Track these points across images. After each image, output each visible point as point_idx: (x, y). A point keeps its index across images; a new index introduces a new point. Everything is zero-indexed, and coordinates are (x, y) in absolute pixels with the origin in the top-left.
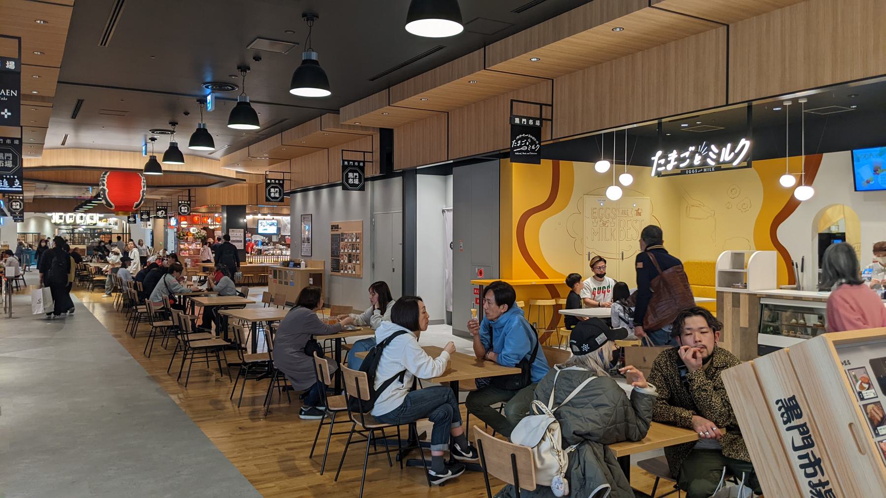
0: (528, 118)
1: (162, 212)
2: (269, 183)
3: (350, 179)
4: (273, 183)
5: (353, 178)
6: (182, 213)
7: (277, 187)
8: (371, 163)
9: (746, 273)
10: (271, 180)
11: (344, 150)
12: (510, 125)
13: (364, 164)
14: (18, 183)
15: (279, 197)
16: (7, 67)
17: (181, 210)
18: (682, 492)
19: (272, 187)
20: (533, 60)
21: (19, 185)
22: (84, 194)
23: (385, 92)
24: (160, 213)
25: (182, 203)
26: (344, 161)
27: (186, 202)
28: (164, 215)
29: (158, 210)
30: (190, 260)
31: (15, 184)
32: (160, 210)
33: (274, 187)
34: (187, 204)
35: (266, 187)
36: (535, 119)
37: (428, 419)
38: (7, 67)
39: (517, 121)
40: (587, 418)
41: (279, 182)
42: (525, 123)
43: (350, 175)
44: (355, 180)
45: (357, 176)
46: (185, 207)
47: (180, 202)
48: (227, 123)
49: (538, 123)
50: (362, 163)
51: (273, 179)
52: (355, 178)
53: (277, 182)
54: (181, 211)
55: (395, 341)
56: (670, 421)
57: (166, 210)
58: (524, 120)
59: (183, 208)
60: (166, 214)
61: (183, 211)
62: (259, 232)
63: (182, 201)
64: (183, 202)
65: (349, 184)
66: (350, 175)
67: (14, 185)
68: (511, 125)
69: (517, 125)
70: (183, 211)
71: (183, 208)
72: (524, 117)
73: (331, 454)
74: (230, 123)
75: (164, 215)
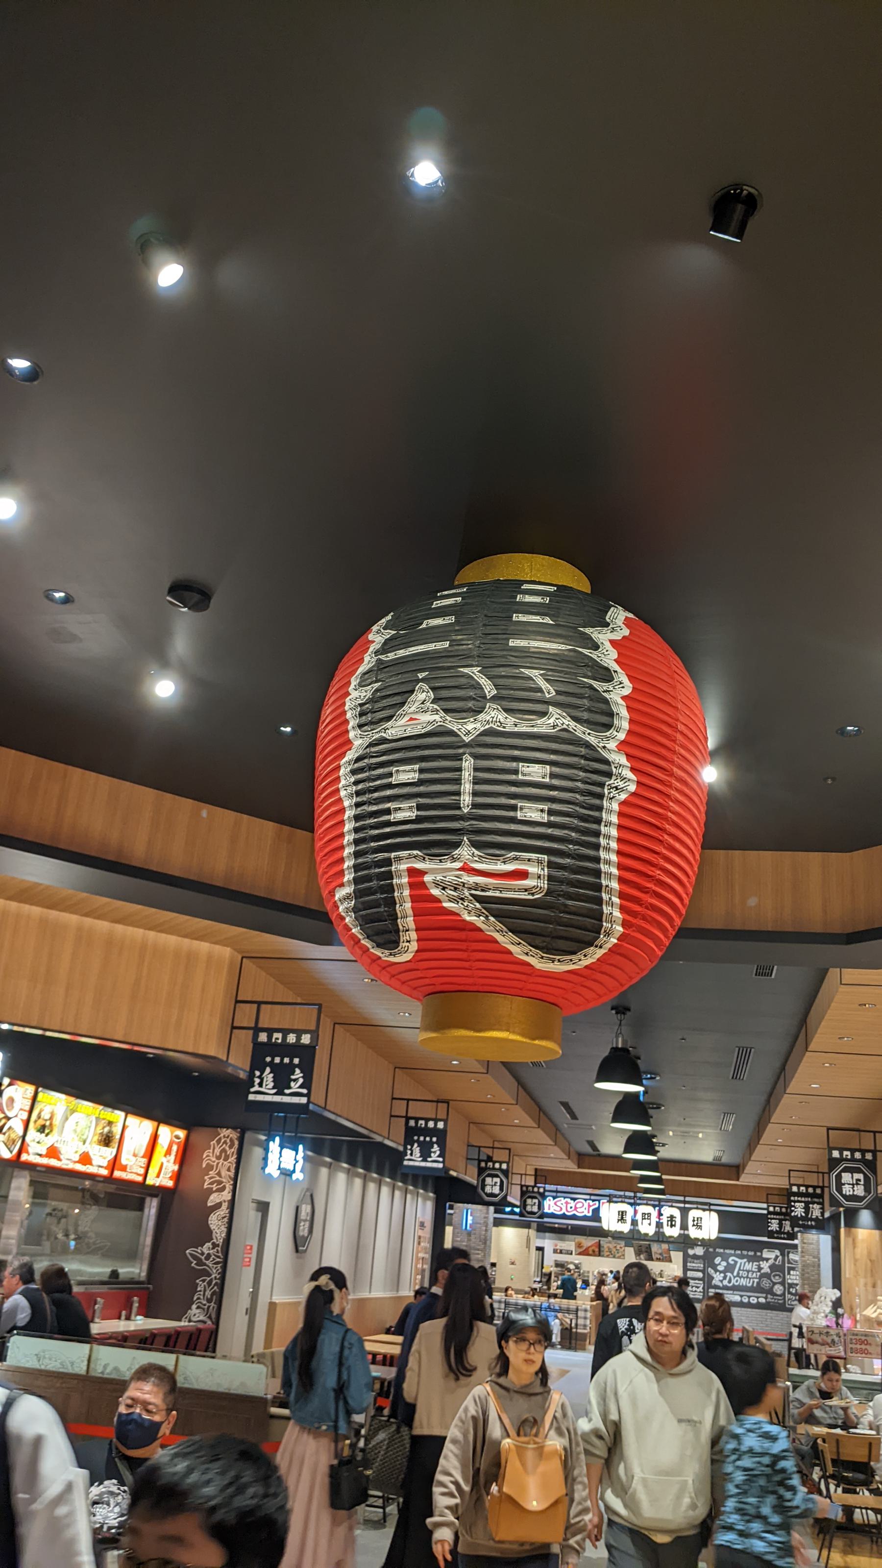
2: (836, 1159)
4: (847, 1160)
5: (853, 1185)
6: (845, 1197)
7: (859, 1171)
9: (590, 1230)
13: (875, 1156)
14: (438, 1153)
15: (864, 1197)
16: (302, 1041)
17: (840, 1185)
19: (845, 1170)
21: (439, 1156)
22: (817, 1473)
25: (841, 1160)
27: (858, 1155)
31: (292, 1084)
33: (852, 1170)
34: (863, 1161)
38: (302, 1041)
41: (863, 1155)
44: (855, 1188)
45: (860, 1180)
46: (857, 1176)
47: (836, 1154)
48: (594, 1075)
50: (870, 1154)
51: (847, 1150)
52: (857, 1184)
53: (858, 1155)
54: (839, 1190)
56: (316, 1147)
59: (846, 1177)
61: (847, 1190)
63: (841, 1150)
64: (846, 1154)
67: (290, 1088)
70: (847, 1190)
71: (846, 1177)
73: (872, 1361)
74: (600, 1079)
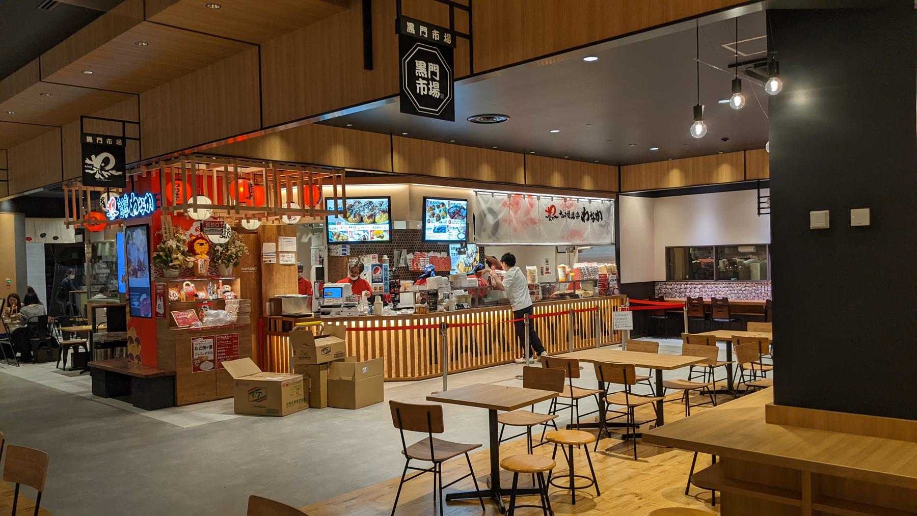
0: (431, 27)
1: (106, 161)
3: (421, 81)
8: (6, 171)
10: (94, 136)
11: (61, 129)
12: (81, 144)
18: (590, 475)
20: (47, 95)
23: (35, 63)
24: (96, 161)
26: (84, 135)
27: (436, 35)
28: (111, 170)
29: (90, 150)
30: (210, 341)
32: (96, 149)
35: (403, 51)
36: (442, 31)
37: (89, 373)
39: (411, 28)
40: (607, 450)
42: (426, 36)
43: (421, 67)
49: (448, 39)
55: (691, 457)
57: (119, 153)
58: (423, 29)
60: (120, 166)
62: (82, 241)
65: (418, 96)
66: (421, 67)
68: (82, 144)
69: (89, 144)
72: (424, 24)
75: (111, 170)
